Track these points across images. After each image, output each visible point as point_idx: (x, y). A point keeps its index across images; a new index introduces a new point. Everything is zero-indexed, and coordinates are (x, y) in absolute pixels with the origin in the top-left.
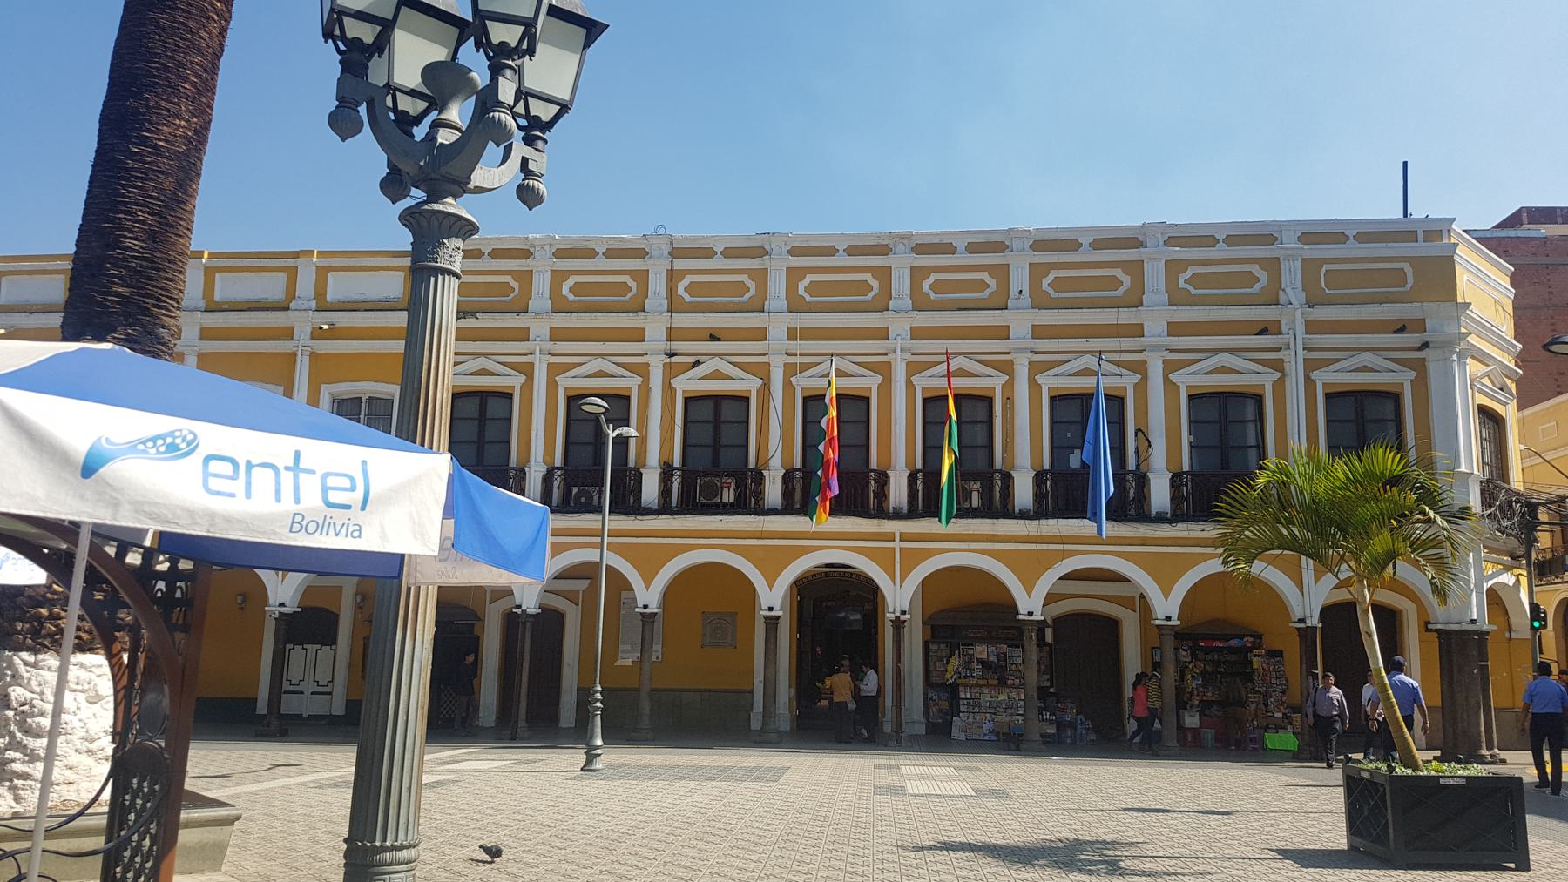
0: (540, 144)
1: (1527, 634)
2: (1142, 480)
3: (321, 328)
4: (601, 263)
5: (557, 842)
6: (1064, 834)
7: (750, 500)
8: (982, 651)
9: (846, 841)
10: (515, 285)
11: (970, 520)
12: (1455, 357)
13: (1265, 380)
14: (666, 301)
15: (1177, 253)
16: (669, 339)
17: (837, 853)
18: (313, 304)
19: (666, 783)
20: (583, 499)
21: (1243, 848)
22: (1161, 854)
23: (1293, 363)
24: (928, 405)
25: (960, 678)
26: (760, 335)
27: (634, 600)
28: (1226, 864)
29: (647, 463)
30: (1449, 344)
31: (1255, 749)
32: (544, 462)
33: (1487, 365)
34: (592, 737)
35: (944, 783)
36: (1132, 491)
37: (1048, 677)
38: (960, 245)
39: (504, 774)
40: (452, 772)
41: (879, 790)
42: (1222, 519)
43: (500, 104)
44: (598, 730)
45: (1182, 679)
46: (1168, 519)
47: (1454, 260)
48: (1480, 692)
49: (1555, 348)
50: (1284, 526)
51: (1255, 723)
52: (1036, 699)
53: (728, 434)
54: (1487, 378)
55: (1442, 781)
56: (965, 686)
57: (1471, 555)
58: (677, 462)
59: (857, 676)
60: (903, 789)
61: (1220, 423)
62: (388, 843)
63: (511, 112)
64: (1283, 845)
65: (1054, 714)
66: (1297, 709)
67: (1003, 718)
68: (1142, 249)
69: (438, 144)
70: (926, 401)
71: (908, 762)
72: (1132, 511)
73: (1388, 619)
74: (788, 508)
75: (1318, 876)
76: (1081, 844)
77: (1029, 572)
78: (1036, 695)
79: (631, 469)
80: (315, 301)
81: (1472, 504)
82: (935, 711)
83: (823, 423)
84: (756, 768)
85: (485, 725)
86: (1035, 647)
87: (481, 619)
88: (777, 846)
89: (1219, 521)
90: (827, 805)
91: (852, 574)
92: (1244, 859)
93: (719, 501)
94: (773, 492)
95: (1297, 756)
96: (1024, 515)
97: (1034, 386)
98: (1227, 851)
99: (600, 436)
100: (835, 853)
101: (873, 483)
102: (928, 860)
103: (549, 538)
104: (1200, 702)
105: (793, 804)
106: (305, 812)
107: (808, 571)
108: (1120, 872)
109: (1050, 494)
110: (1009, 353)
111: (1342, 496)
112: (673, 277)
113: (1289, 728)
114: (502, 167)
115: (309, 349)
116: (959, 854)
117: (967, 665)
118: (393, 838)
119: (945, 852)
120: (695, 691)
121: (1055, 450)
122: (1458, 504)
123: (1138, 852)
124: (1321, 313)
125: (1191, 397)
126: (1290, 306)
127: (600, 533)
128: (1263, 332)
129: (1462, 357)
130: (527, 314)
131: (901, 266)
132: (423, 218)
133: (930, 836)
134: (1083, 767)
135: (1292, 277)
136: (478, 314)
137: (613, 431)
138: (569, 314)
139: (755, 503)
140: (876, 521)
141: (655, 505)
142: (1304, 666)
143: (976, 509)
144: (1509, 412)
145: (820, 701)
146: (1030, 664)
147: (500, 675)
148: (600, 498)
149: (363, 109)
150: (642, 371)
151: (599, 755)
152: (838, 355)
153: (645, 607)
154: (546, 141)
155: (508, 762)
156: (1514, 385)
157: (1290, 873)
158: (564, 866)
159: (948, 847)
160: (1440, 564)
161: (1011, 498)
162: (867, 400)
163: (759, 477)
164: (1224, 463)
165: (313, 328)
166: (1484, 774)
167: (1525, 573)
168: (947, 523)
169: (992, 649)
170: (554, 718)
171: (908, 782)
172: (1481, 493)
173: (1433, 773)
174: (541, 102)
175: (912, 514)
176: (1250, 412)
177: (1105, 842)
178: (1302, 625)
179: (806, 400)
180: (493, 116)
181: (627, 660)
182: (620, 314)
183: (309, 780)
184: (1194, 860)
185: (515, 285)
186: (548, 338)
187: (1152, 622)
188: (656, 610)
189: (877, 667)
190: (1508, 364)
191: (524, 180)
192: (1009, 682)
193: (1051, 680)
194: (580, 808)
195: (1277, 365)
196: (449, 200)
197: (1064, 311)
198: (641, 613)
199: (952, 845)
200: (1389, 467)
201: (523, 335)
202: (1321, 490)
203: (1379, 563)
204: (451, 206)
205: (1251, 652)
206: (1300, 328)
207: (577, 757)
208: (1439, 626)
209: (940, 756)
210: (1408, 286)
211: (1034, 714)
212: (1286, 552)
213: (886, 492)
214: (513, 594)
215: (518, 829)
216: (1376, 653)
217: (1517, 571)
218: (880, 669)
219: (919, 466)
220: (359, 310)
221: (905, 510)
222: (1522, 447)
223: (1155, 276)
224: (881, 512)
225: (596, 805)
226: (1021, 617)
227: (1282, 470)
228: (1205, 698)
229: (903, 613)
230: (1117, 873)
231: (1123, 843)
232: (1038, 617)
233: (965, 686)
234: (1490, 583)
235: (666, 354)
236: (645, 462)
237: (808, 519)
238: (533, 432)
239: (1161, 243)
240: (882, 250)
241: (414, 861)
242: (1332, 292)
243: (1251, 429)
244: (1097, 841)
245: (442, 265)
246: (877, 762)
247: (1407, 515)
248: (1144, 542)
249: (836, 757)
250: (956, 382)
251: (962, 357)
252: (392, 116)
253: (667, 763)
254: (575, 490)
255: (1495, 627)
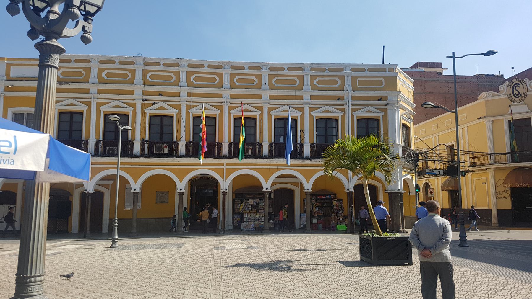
0: (90, 21)
1: (414, 194)
2: (302, 146)
3: (8, 87)
4: (117, 66)
5: (101, 272)
6: (274, 259)
7: (174, 152)
8: (251, 202)
9: (204, 266)
10: (84, 73)
11: (248, 159)
12: (396, 108)
13: (338, 115)
14: (142, 81)
15: (314, 73)
16: (144, 95)
17: (200, 270)
18: (5, 78)
19: (141, 250)
20: (111, 152)
21: (329, 261)
22: (304, 264)
23: (348, 109)
24: (235, 121)
25: (244, 210)
26: (177, 94)
27: (131, 188)
28: (323, 266)
29: (135, 139)
30: (394, 104)
31: (334, 230)
32: (95, 138)
33: (405, 111)
34: (114, 236)
35: (238, 245)
36: (299, 149)
37: (272, 209)
38: (246, 67)
39: (81, 249)
40: (61, 249)
41: (216, 248)
42: (324, 158)
43: (74, 6)
44: (116, 233)
45: (312, 209)
46: (309, 158)
47: (397, 78)
48: (400, 211)
49: (425, 106)
50: (342, 160)
51: (334, 222)
52: (268, 216)
53: (166, 129)
54: (405, 115)
55: (388, 239)
56: (246, 213)
57: (399, 170)
58: (147, 138)
59: (211, 212)
60: (224, 247)
61: (325, 128)
62: (32, 275)
63: (78, 9)
64: (341, 260)
65: (273, 221)
66: (346, 217)
67: (257, 223)
68: (303, 72)
69: (50, 19)
70: (235, 119)
71: (226, 239)
72: (299, 156)
73: (373, 189)
74: (187, 155)
75: (351, 269)
76: (279, 262)
77: (267, 175)
78: (268, 215)
79: (129, 141)
80: (6, 77)
81: (399, 154)
82: (236, 221)
83: (201, 126)
84: (174, 244)
85: (74, 233)
86: (268, 199)
87: (72, 195)
88: (180, 269)
89: (323, 159)
90: (211, 257)
91: (209, 177)
92: (329, 264)
93: (162, 152)
94: (182, 150)
95: (346, 232)
96: (265, 157)
97: (269, 115)
98: (324, 262)
99: (117, 129)
100: (200, 270)
101: (217, 146)
102: (231, 270)
103: (91, 166)
104: (317, 215)
105: (186, 255)
106: (4, 265)
107: (194, 177)
108: (291, 270)
109: (274, 150)
110: (262, 104)
111: (360, 151)
112: (145, 72)
113: (344, 223)
114: (75, 29)
115: (3, 95)
116: (241, 267)
117: (246, 206)
118: (35, 273)
119: (236, 267)
120: (153, 218)
121: (276, 136)
122: (395, 153)
123: (296, 264)
124: (357, 94)
125: (317, 120)
126: (348, 91)
127: (117, 163)
128: (339, 99)
129: (398, 108)
130: (89, 84)
131: (227, 72)
132: (43, 47)
133: (232, 262)
134: (281, 237)
135: (348, 82)
136: (70, 83)
137: (122, 127)
138: (105, 84)
139: (176, 153)
140: (218, 159)
141: (138, 154)
142: (349, 204)
143: (250, 155)
144: (411, 126)
145: (198, 220)
146: (266, 205)
147: (79, 215)
148: (117, 151)
149: (20, 5)
150: (134, 106)
151: (117, 242)
152: (205, 102)
153: (135, 190)
154: (92, 20)
155: (83, 245)
156: (413, 117)
157: (343, 269)
158: (103, 280)
159: (237, 265)
160: (388, 172)
161: (262, 152)
162: (215, 118)
163: (177, 144)
164: (326, 141)
165: (5, 87)
166: (400, 236)
167: (414, 175)
168: (241, 160)
169: (255, 201)
170: (101, 229)
171: (226, 245)
172: (402, 150)
173: (385, 236)
174: (91, 6)
175: (230, 157)
176: (334, 124)
177: (287, 261)
178: (348, 191)
179: (194, 118)
180: (71, 10)
181: (128, 209)
182: (125, 85)
183: (5, 253)
184: (314, 265)
185: (84, 73)
186: (97, 92)
187: (304, 191)
188: (139, 191)
189: (217, 208)
190: (411, 110)
191: (83, 34)
192: (260, 211)
193: (273, 210)
194: (109, 260)
195: (343, 110)
196: (54, 40)
197: (279, 90)
198: (133, 192)
199: (239, 265)
200: (374, 142)
201: (87, 91)
202: (354, 149)
203: (370, 172)
204: (54, 42)
205: (333, 200)
206: (350, 98)
207: (109, 243)
208: (389, 191)
209: (237, 236)
210: (383, 86)
211: (267, 221)
212: (343, 168)
213: (221, 150)
214: (84, 186)
215: (86, 268)
216: (369, 200)
217: (412, 174)
218: (218, 209)
219: (232, 141)
220: (23, 81)
221: (227, 156)
222: (415, 136)
223: (307, 80)
224: (220, 157)
225: (115, 259)
226: (264, 190)
227: (342, 143)
228: (319, 214)
229: (226, 190)
230: (290, 270)
231: (292, 261)
232: (269, 190)
233: (246, 213)
234: (404, 178)
235: (142, 100)
236: (135, 138)
237: (198, 159)
238: (91, 127)
239: (309, 69)
240: (220, 67)
241: (43, 281)
242: (360, 87)
243: (334, 130)
244: (285, 261)
245: (51, 64)
246: (216, 239)
247: (379, 157)
248: (302, 165)
249: (210, 238)
250: (245, 113)
251: (247, 105)
252: (32, 8)
253: (142, 244)
254: (107, 148)
255: (405, 192)
